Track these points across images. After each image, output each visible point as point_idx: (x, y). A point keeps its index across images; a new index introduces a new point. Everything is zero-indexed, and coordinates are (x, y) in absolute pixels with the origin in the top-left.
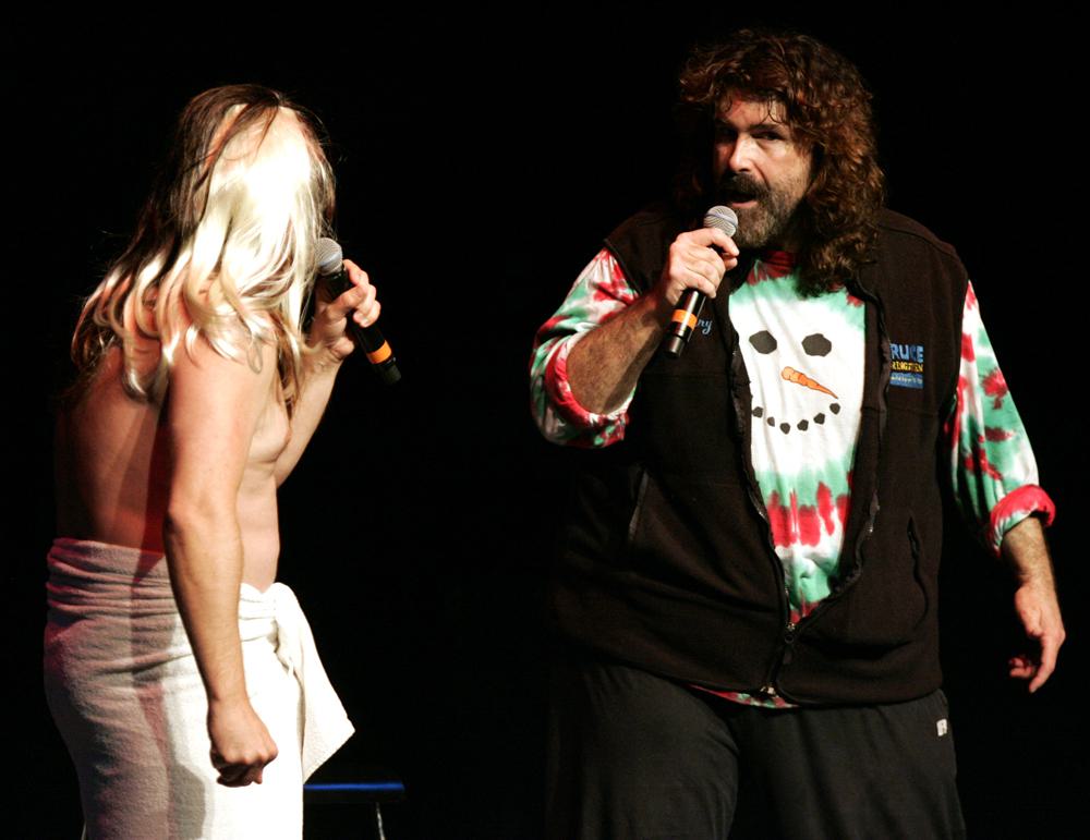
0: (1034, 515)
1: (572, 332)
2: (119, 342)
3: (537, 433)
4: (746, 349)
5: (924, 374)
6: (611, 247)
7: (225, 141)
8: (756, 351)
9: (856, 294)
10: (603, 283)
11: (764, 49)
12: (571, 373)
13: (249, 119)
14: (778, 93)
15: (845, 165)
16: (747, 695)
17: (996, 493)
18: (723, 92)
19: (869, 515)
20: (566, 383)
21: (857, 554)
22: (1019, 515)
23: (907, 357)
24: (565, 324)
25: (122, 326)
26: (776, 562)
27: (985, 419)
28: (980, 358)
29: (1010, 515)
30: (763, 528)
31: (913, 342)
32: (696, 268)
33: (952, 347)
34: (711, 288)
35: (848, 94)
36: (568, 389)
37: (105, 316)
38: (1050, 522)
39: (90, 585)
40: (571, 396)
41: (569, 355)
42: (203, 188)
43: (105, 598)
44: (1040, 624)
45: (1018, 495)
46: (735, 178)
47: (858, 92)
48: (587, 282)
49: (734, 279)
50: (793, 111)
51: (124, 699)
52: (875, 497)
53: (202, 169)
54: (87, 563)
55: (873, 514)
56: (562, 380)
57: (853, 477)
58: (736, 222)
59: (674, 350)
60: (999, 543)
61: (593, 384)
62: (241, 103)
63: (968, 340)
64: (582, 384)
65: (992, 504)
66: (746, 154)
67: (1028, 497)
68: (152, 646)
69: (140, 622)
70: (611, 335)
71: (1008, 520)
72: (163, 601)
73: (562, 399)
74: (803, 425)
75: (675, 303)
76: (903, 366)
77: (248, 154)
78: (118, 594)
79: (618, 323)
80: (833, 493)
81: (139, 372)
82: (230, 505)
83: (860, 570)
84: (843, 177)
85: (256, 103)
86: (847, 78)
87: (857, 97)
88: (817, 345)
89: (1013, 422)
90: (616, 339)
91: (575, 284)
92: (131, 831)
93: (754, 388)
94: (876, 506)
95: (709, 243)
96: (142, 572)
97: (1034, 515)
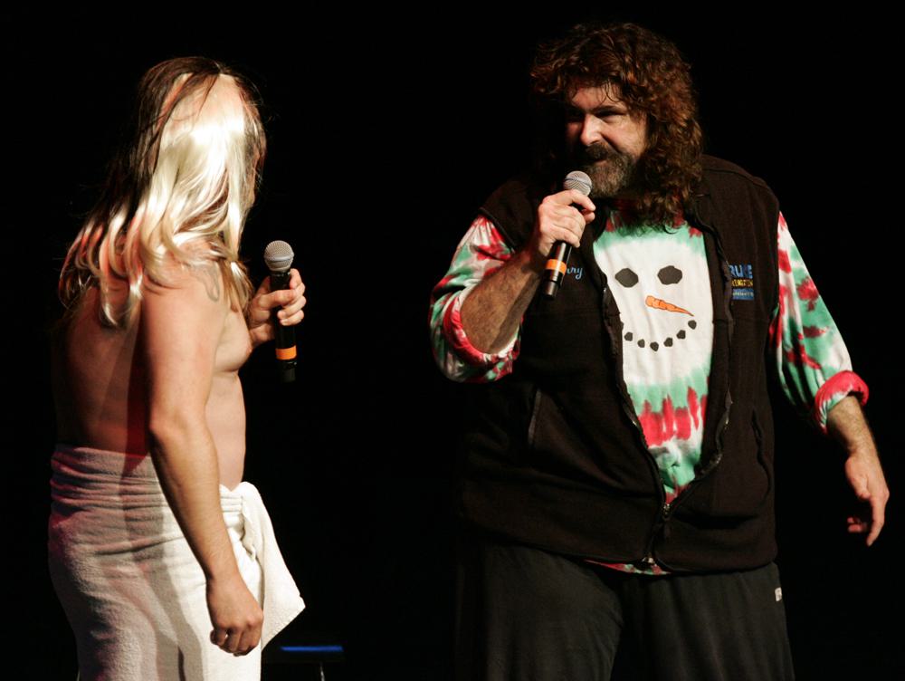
0: (851, 394)
1: (462, 288)
2: (96, 283)
3: (442, 374)
4: (614, 286)
5: (754, 288)
6: (488, 213)
7: (174, 105)
8: (621, 286)
9: (696, 225)
10: (483, 246)
11: (597, 39)
12: (465, 320)
13: (194, 85)
14: (612, 78)
15: (672, 128)
16: (631, 565)
17: (816, 380)
18: (569, 82)
20: (462, 330)
21: (718, 441)
22: (839, 396)
23: (741, 275)
24: (455, 281)
25: (98, 268)
27: (803, 319)
28: (795, 271)
29: (831, 397)
30: (636, 435)
32: (561, 224)
33: (770, 261)
34: (575, 239)
35: (669, 67)
36: (464, 335)
37: (85, 259)
38: (865, 400)
39: (87, 484)
41: (462, 309)
42: (155, 146)
43: (99, 494)
44: (867, 487)
45: (835, 381)
46: (587, 150)
47: (678, 64)
48: (468, 245)
49: (594, 231)
50: (626, 91)
52: (729, 393)
53: (155, 129)
54: (84, 467)
55: (728, 408)
56: (457, 328)
57: (712, 380)
58: (590, 183)
59: (550, 293)
60: (825, 421)
61: (484, 328)
62: (188, 72)
63: (785, 255)
64: (474, 330)
65: (815, 390)
66: (593, 130)
67: (844, 381)
68: (138, 534)
69: (132, 513)
70: (496, 287)
71: (829, 401)
72: (147, 496)
74: (669, 342)
75: (546, 255)
76: (740, 283)
77: (193, 114)
78: (109, 491)
79: (500, 276)
81: (113, 304)
82: (204, 415)
84: (671, 139)
85: (201, 71)
86: (668, 54)
87: (678, 68)
88: (670, 275)
89: (826, 320)
90: (501, 289)
91: (459, 247)
93: (623, 317)
94: (729, 401)
95: (570, 202)
96: (127, 472)
97: (851, 394)
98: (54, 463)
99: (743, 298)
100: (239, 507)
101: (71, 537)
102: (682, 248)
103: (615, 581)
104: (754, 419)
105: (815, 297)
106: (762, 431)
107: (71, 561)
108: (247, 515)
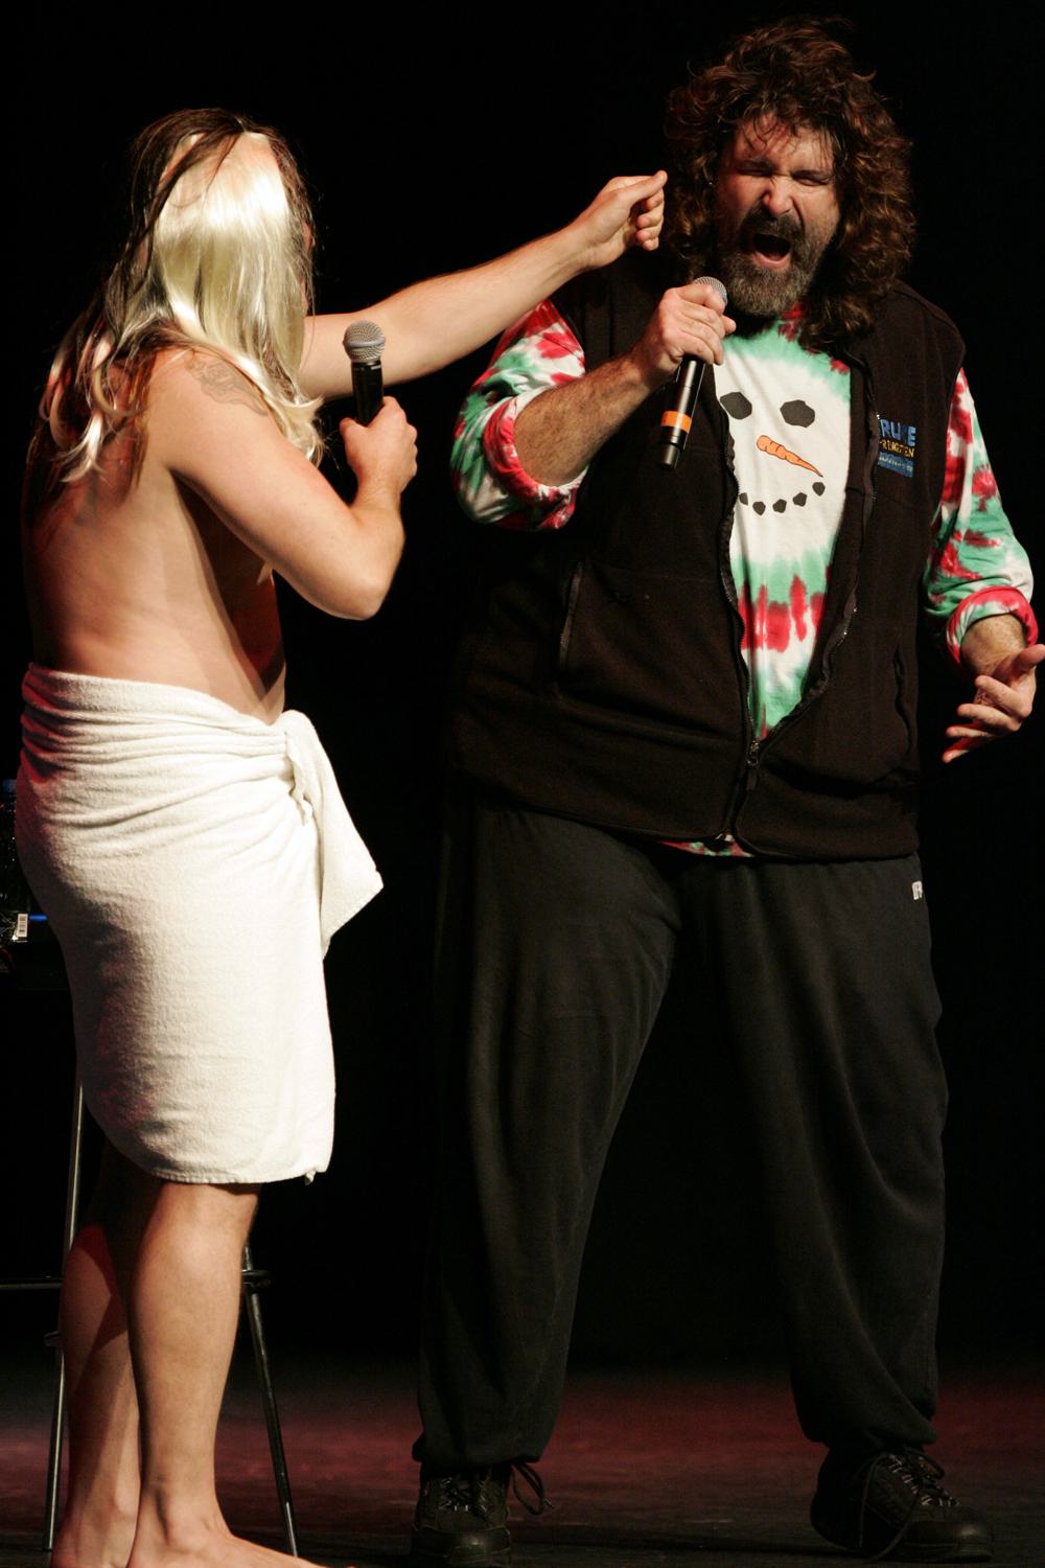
16: (700, 844)
19: (843, 616)
21: (825, 663)
26: (740, 667)
31: (906, 424)
36: (515, 454)
40: (518, 462)
51: (106, 857)
54: (56, 698)
57: (833, 571)
59: (669, 461)
68: (136, 795)
73: (506, 465)
74: (780, 506)
76: (894, 447)
80: (808, 591)
83: (825, 683)
88: (798, 413)
92: (134, 1010)
98: (27, 694)
99: (894, 469)
100: (282, 747)
101: (46, 803)
102: (826, 387)
103: (669, 866)
104: (897, 654)
105: (873, 134)
106: (906, 670)
107: (48, 837)
108: (295, 758)
